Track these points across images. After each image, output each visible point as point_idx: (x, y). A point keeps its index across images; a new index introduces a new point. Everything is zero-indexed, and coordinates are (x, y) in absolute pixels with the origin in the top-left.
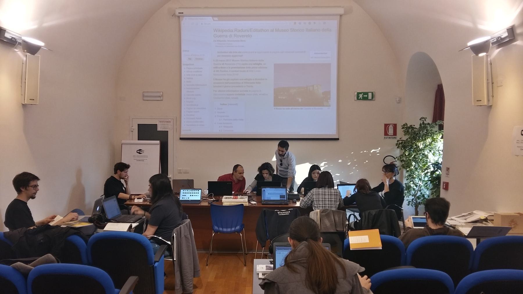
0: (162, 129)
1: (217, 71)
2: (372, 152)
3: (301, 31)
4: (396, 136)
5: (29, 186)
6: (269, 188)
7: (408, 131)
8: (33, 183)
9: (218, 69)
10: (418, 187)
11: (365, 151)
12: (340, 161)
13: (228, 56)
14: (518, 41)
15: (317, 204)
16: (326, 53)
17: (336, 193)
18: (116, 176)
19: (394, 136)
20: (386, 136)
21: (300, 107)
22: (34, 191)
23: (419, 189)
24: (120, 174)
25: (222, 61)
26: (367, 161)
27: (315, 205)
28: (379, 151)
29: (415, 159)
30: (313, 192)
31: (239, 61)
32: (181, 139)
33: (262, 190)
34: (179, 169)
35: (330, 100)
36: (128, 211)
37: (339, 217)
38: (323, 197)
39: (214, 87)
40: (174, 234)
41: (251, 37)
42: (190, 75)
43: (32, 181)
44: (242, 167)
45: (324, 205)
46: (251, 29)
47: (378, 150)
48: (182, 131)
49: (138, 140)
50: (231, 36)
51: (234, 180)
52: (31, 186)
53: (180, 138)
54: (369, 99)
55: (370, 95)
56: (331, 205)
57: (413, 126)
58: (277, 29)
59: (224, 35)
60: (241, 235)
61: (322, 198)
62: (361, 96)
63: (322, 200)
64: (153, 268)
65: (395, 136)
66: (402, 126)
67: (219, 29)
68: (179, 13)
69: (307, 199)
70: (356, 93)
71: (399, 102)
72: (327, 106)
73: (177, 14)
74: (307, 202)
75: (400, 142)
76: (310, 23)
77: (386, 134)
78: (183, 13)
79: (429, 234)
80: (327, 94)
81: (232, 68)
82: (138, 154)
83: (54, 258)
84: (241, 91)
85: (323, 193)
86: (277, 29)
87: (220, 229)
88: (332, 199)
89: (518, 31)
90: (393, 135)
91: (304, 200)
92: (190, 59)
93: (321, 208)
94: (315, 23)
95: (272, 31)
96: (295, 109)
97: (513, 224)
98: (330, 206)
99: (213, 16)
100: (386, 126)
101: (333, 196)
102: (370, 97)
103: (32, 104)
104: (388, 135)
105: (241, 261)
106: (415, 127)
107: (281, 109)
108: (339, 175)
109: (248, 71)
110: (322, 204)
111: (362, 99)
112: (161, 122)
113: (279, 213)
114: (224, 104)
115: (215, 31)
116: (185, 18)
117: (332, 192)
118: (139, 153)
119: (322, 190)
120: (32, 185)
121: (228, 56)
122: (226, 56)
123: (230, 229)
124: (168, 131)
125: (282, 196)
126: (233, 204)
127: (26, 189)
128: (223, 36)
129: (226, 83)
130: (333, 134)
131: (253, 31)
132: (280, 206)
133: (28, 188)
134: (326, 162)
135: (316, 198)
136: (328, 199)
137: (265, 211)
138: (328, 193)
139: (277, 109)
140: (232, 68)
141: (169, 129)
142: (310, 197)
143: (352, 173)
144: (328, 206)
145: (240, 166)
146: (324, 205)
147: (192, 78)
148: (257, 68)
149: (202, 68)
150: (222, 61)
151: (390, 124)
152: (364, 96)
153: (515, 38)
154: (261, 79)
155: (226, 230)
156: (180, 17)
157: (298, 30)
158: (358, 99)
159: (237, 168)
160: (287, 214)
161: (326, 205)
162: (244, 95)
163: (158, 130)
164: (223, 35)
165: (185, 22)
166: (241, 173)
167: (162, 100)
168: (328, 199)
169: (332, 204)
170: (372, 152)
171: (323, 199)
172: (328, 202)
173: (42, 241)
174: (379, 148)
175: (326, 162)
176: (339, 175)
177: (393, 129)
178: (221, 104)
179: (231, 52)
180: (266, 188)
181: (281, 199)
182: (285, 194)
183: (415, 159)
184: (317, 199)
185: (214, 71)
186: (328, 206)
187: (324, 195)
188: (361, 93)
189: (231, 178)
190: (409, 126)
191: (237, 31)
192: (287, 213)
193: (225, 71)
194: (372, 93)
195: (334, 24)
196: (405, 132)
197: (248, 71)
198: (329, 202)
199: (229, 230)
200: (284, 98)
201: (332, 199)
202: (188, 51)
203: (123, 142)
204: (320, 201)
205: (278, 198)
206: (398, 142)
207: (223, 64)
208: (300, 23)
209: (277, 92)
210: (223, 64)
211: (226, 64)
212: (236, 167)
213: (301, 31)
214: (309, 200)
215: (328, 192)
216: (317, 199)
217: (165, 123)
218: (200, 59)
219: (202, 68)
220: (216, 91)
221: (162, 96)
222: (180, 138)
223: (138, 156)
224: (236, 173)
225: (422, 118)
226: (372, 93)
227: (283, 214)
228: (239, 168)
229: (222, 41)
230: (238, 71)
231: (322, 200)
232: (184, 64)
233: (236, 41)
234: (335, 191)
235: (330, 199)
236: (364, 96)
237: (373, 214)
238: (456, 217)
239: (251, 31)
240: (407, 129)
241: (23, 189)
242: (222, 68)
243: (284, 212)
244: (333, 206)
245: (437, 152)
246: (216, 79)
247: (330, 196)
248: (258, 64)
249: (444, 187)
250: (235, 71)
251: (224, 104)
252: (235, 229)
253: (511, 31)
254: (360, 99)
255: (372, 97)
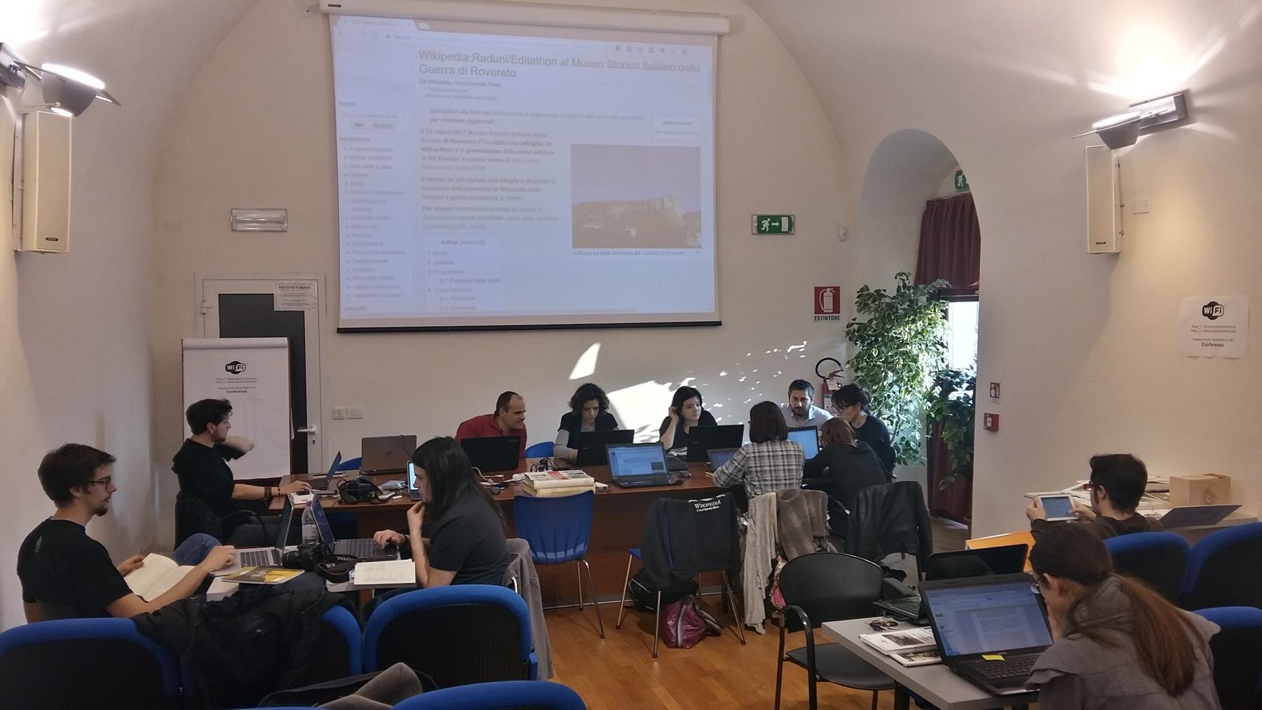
0: (286, 306)
1: (432, 158)
2: (789, 350)
3: (631, 66)
4: (839, 313)
5: (93, 483)
6: (624, 448)
7: (866, 305)
8: (101, 473)
9: (433, 154)
10: (894, 424)
11: (776, 350)
12: (723, 374)
13: (457, 121)
14: (1195, 122)
15: (759, 481)
16: (690, 124)
17: (798, 451)
18: (205, 441)
19: (834, 315)
20: (818, 315)
21: (634, 250)
22: (104, 495)
23: (896, 429)
24: (216, 432)
25: (441, 132)
26: (780, 373)
27: (754, 483)
28: (803, 349)
29: (890, 365)
30: (747, 453)
31: (486, 134)
32: (341, 331)
33: (610, 452)
34: (336, 408)
35: (700, 232)
36: (264, 527)
37: (817, 506)
38: (772, 464)
39: (424, 197)
40: (514, 579)
41: (515, 76)
42: (359, 167)
43: (98, 466)
44: (521, 398)
45: (776, 480)
46: (514, 58)
47: (802, 347)
48: (342, 310)
49: (221, 337)
50: (463, 71)
51: (502, 430)
52: (100, 482)
53: (338, 329)
54: (782, 230)
55: (785, 221)
56: (790, 479)
57: (882, 292)
58: (576, 60)
59: (447, 69)
60: (587, 564)
61: (770, 466)
62: (766, 224)
63: (771, 470)
64: (529, 669)
65: (837, 315)
66: (858, 292)
67: (434, 52)
68: (329, 5)
69: (734, 469)
70: (755, 218)
71: (844, 237)
72: (693, 247)
73: (324, 7)
74: (732, 476)
75: (856, 329)
76: (651, 50)
77: (818, 310)
78: (340, 6)
79: (1115, 533)
80: (693, 219)
81: (468, 151)
82: (230, 373)
83: (412, 671)
84: (492, 210)
85: (771, 454)
86: (576, 60)
87: (548, 557)
88: (792, 465)
89: (1198, 103)
90: (832, 311)
91: (726, 471)
92: (358, 125)
93: (783, 488)
94: (684, 52)
95: (564, 63)
96: (623, 253)
97: (1209, 497)
98: (788, 482)
99: (418, 19)
100: (819, 291)
101: (751, 462)
102: (785, 227)
103: (43, 253)
104: (822, 312)
105: (580, 626)
106: (886, 294)
107: (590, 253)
108: (721, 405)
109: (507, 160)
110: (771, 480)
111: (767, 230)
112: (283, 287)
113: (697, 506)
114: (449, 242)
115: (422, 58)
116: (342, 17)
117: (790, 451)
118: (233, 372)
119: (767, 446)
120: (101, 477)
121: (457, 121)
122: (451, 121)
123: (564, 552)
124: (304, 312)
125: (655, 466)
126: (560, 493)
127: (86, 492)
128: (444, 70)
129: (454, 189)
130: (709, 311)
131: (517, 61)
132: (667, 489)
133: (90, 488)
134: (693, 379)
135: (756, 467)
136: (782, 468)
137: (666, 503)
138: (781, 453)
139: (580, 253)
140: (468, 151)
141: (306, 306)
142: (739, 464)
143: (749, 400)
144: (784, 482)
145: (514, 396)
146: (774, 482)
147: (367, 176)
148: (530, 152)
149: (390, 150)
150: (441, 132)
151: (826, 288)
152: (773, 224)
153: (1187, 116)
154: (541, 181)
155: (555, 557)
156: (330, 16)
157: (625, 66)
158: (760, 231)
159: (509, 400)
160: (715, 508)
161: (780, 480)
162: (502, 218)
163: (275, 310)
164: (443, 68)
165: (344, 29)
166: (518, 413)
167: (285, 231)
168: (782, 468)
169: (791, 477)
170: (789, 350)
171: (773, 468)
172: (783, 474)
173: (259, 631)
174: (805, 343)
175: (693, 379)
176: (721, 405)
177: (832, 298)
178: (443, 242)
179: (464, 112)
180: (618, 448)
181: (656, 471)
182: (663, 460)
183: (890, 365)
184: (758, 469)
185: (423, 158)
186: (784, 482)
187: (774, 459)
188: (765, 217)
189: (493, 424)
190: (872, 291)
191: (480, 59)
192: (715, 506)
193: (450, 159)
194: (789, 217)
195: (704, 55)
196: (861, 303)
197: (507, 160)
198: (784, 473)
199: (561, 555)
200: (597, 227)
201: (792, 465)
202: (354, 104)
203: (187, 342)
204: (765, 474)
205: (648, 470)
206: (851, 328)
207: (446, 141)
208: (629, 49)
209: (579, 212)
210: (446, 141)
211: (452, 141)
212: (505, 399)
213: (631, 66)
214: (738, 471)
215: (782, 451)
216: (758, 469)
217: (295, 291)
218: (383, 126)
219: (390, 150)
220: (429, 209)
221: (286, 218)
222: (338, 329)
223: (230, 381)
224: (507, 412)
225: (899, 274)
226: (789, 217)
227: (706, 509)
228: (513, 401)
229: (443, 83)
230: (483, 160)
231: (771, 470)
232: (344, 139)
233: (477, 84)
234: (796, 447)
235: (786, 468)
236: (773, 224)
237: (885, 492)
238: (1073, 490)
239: (514, 61)
240: (867, 298)
241: (78, 491)
242: (442, 150)
243: (708, 504)
244: (794, 481)
245: (933, 348)
246: (430, 179)
247: (786, 460)
248: (534, 145)
249: (989, 425)
250: (477, 160)
251: (449, 242)
252: (574, 551)
253: (1182, 99)
254: (764, 232)
255: (790, 228)
